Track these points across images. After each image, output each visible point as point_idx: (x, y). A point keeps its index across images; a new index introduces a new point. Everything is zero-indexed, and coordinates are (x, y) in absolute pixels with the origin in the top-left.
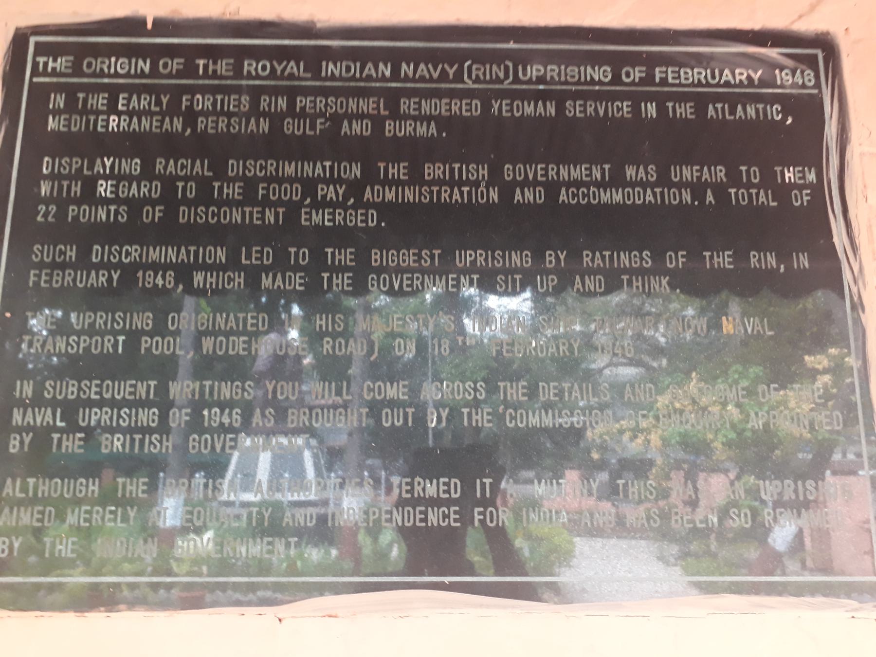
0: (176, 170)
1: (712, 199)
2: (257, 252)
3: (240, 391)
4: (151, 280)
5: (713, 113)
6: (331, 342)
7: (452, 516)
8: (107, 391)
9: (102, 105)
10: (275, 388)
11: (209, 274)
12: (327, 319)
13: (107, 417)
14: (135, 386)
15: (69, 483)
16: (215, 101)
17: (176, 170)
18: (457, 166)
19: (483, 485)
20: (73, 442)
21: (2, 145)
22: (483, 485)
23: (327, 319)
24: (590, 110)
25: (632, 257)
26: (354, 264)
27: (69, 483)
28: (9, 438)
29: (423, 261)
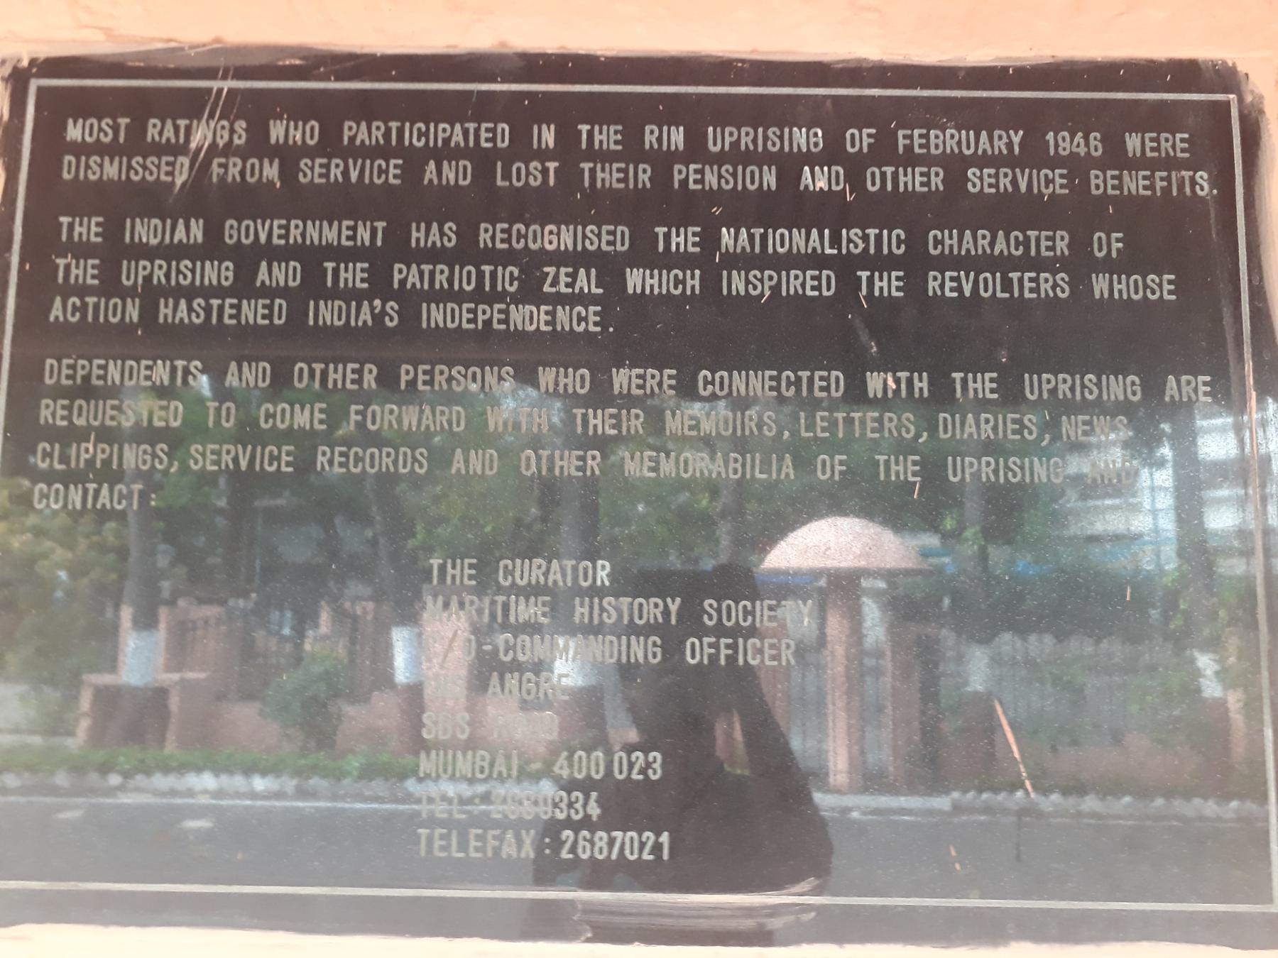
0: (111, 501)
3: (148, 457)
7: (284, 458)
8: (80, 415)
14: (642, 377)
15: (96, 406)
16: (388, 130)
17: (111, 501)
18: (487, 269)
21: (3, 136)
24: (1005, 183)
25: (140, 453)
27: (96, 406)
28: (38, 407)
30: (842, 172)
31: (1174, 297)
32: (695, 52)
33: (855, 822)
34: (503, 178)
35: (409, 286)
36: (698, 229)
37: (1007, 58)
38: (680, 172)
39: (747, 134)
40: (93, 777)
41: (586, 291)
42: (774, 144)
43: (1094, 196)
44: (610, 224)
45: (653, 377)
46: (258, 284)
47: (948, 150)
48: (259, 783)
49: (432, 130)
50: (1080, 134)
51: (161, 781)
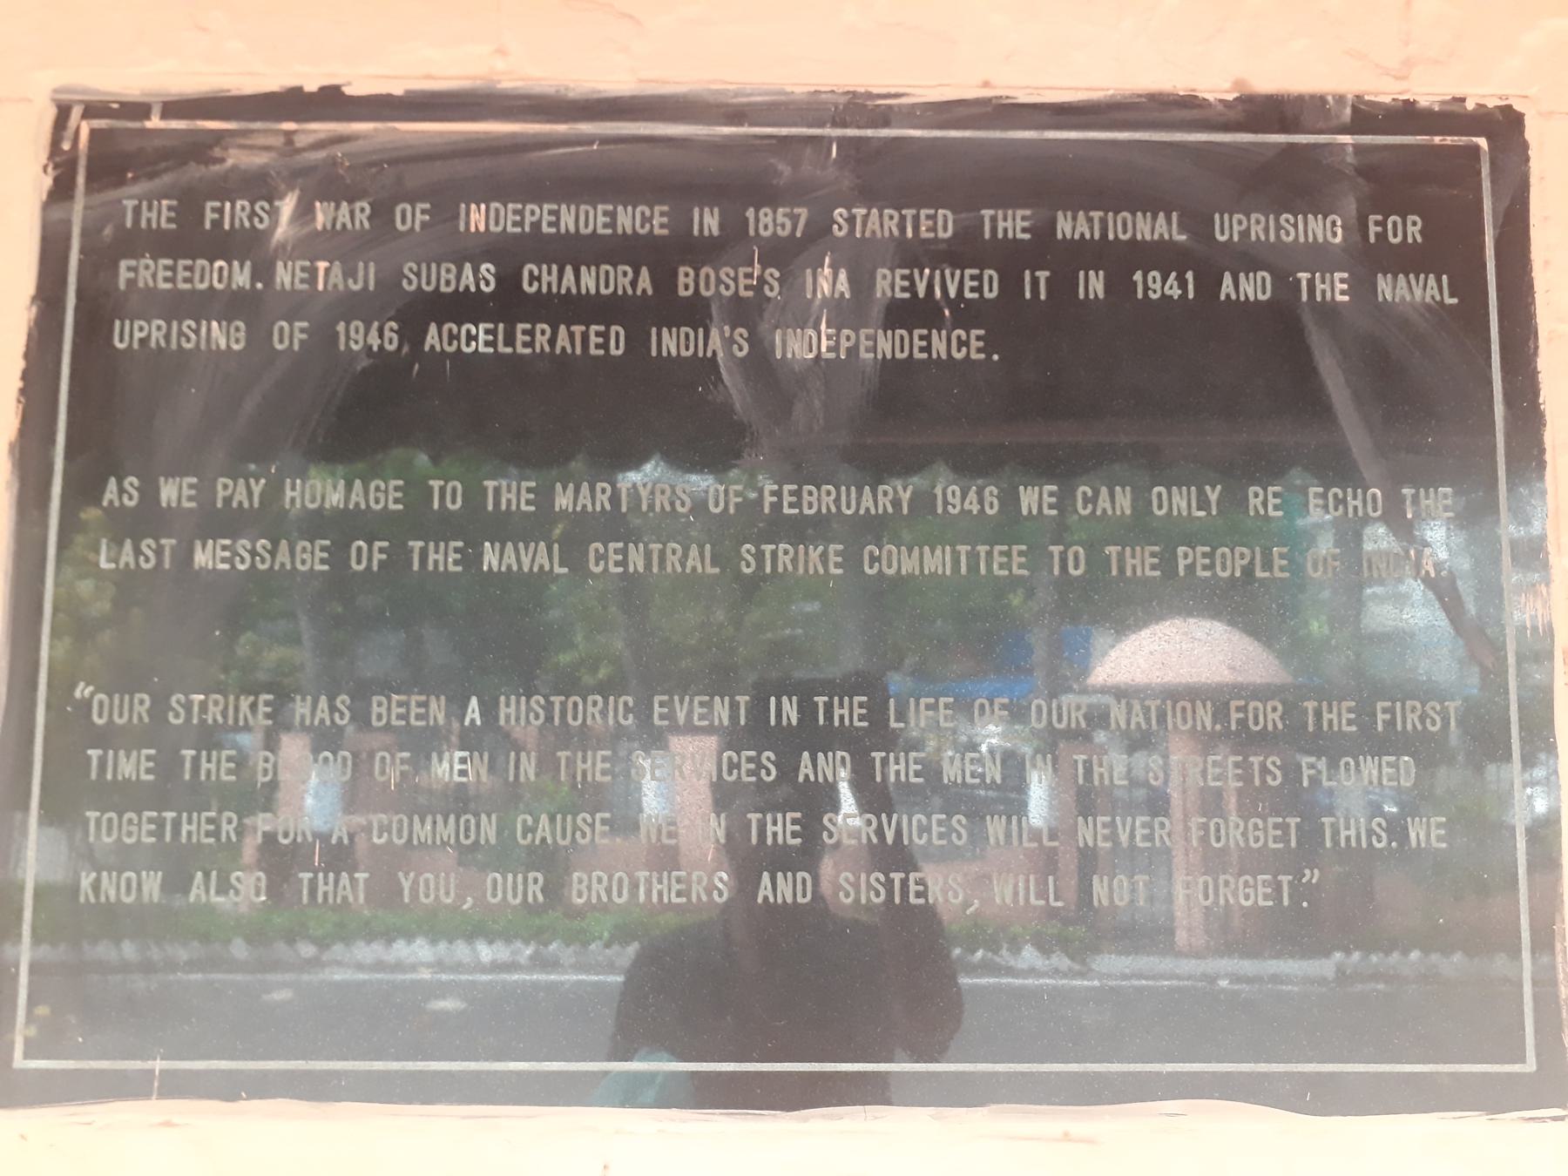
1: (477, 716)
2: (525, 332)
4: (360, 337)
9: (1439, 839)
10: (415, 882)
16: (903, 218)
19: (1035, 282)
20: (446, 554)
22: (1035, 282)
29: (763, 772)
30: (622, 332)
33: (1223, 990)
35: (235, 505)
39: (1258, 222)
40: (281, 948)
41: (363, 506)
42: (1288, 234)
43: (614, 357)
44: (923, 328)
45: (786, 552)
46: (1223, 297)
48: (485, 952)
51: (366, 952)
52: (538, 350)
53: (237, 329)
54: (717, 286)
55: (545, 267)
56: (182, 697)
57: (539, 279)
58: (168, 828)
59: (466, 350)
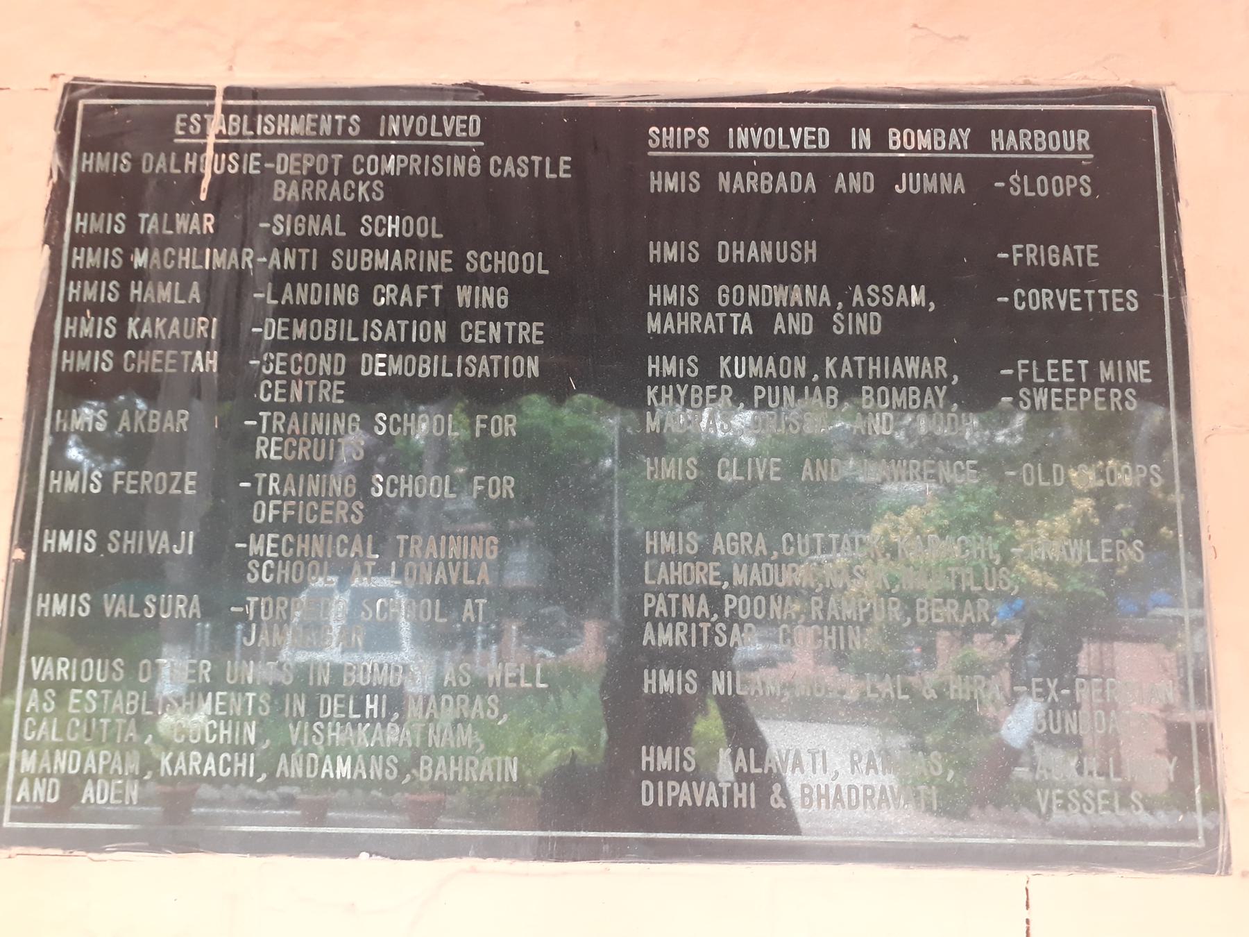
2: (1053, 366)
5: (849, 370)
6: (701, 391)
11: (742, 260)
12: (883, 362)
13: (417, 166)
23: (883, 362)
26: (1097, 264)
31: (1149, 381)
32: (1188, 308)
34: (176, 167)
36: (569, 159)
37: (1183, 271)
38: (760, 392)
47: (1045, 307)
49: (103, 295)
50: (170, 412)
52: (491, 341)
53: (279, 194)
54: (373, 222)
55: (496, 253)
56: (525, 158)
57: (492, 262)
58: (260, 484)
59: (378, 234)
